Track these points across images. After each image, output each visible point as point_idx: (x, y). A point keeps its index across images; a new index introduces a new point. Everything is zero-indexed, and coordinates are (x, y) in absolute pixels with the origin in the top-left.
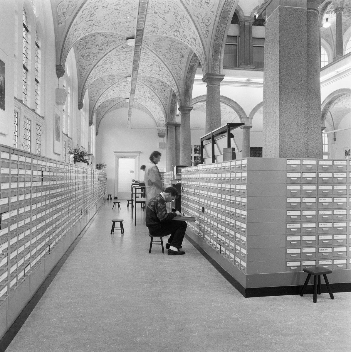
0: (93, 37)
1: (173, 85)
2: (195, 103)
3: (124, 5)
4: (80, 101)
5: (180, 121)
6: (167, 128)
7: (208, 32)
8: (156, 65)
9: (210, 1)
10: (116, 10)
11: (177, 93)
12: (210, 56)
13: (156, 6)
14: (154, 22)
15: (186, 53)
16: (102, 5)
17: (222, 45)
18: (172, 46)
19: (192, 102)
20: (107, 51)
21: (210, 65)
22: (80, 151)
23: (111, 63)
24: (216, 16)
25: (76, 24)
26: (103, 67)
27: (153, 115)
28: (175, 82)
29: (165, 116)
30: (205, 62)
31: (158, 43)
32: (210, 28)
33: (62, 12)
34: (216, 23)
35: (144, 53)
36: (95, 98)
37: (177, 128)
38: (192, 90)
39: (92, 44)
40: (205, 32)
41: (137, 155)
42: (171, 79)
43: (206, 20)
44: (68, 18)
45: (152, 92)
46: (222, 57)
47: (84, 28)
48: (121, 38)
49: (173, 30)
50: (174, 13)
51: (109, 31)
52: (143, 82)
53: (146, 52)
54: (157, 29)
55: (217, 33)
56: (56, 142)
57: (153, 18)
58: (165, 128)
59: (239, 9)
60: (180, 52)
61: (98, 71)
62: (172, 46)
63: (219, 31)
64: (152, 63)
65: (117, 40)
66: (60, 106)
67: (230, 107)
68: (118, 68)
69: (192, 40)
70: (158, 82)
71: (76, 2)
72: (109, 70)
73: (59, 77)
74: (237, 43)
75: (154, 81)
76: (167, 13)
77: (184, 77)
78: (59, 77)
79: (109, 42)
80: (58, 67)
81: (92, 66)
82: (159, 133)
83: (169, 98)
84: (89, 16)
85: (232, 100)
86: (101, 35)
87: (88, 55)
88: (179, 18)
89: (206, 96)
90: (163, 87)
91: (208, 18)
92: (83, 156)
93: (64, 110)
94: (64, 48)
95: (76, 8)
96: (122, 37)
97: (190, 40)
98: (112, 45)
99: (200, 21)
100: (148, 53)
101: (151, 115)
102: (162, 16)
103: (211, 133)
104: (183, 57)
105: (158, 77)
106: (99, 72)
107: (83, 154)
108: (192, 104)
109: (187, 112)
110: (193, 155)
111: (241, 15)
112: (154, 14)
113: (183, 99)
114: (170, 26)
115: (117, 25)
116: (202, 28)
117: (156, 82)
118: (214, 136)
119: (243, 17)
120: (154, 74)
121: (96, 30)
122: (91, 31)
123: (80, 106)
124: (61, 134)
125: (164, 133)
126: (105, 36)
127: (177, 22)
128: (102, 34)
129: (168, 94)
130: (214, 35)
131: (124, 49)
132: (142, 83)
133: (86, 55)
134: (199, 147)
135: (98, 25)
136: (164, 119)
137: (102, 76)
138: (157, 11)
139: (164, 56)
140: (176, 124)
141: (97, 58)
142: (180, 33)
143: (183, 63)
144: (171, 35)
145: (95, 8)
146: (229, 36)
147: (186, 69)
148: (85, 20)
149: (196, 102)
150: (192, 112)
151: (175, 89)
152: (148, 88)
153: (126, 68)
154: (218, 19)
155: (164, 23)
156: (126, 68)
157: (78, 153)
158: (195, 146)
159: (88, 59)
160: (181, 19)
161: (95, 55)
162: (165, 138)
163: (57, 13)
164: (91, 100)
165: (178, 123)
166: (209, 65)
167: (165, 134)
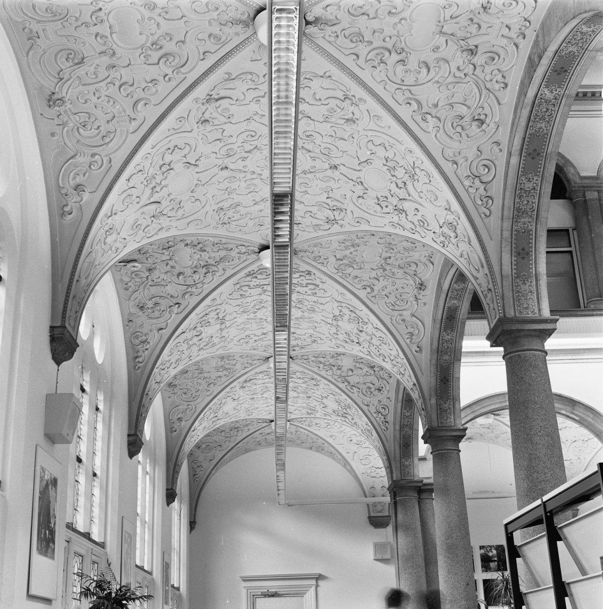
0: (166, 253)
1: (402, 370)
2: (471, 420)
3: (246, 155)
4: (133, 432)
5: (431, 474)
6: (395, 498)
7: (490, 201)
8: (346, 317)
9: (486, 115)
10: (222, 169)
11: (416, 392)
12: (504, 267)
13: (332, 147)
14: (331, 195)
15: (430, 275)
16: (185, 160)
17: (538, 233)
18: (390, 258)
19: (462, 416)
20: (207, 288)
21: (508, 294)
22: (115, 587)
23: (222, 321)
24: (510, 154)
25: (112, 214)
26: (198, 334)
27: (352, 463)
28: (405, 361)
29: (386, 463)
30: (491, 286)
31: (347, 252)
32: (497, 189)
33: (72, 183)
34: (509, 182)
35: (312, 287)
36: (183, 423)
37: (424, 496)
38: (459, 378)
39: (166, 273)
40: (480, 203)
41: (310, 586)
42: (394, 353)
43: (482, 168)
44: (89, 199)
45: (344, 396)
46: (542, 268)
47: (136, 226)
48: (243, 250)
49: (387, 210)
50: (385, 162)
51: (210, 231)
52: (316, 369)
53: (318, 282)
54: (343, 214)
55: (517, 200)
56: (38, 559)
57: (328, 184)
58: (388, 499)
59: (563, 162)
60: (412, 273)
61: (185, 346)
62: (390, 258)
63: (525, 195)
64: (337, 313)
65: (233, 254)
66: (59, 447)
67: (575, 425)
68: (243, 336)
69: (445, 230)
70: (358, 365)
71: (111, 154)
72: (216, 340)
73: (58, 362)
74: (570, 246)
75: (346, 363)
76: (364, 164)
77: (432, 344)
78: (58, 362)
79: (211, 262)
80: (55, 332)
81: (166, 333)
82: (372, 514)
83: (392, 411)
84: (148, 191)
85: (579, 403)
86: (187, 245)
87: (156, 304)
88: (400, 173)
89: (507, 397)
90: (375, 381)
91: (486, 162)
92: (124, 602)
93: (79, 460)
94: (76, 278)
95: (111, 169)
96: (246, 244)
97: (438, 230)
98: (221, 272)
99: (463, 171)
100: (321, 286)
101: (346, 464)
102: (354, 175)
103: (538, 502)
104: (422, 286)
105: (356, 350)
106: (189, 348)
107: (126, 594)
108: (463, 422)
109: (450, 445)
110: (480, 576)
111: (570, 176)
112: (329, 173)
113: (434, 406)
114: (379, 200)
115: (230, 213)
116: (471, 190)
117: (352, 368)
118: (551, 512)
119: (578, 180)
120: (344, 344)
121: (173, 229)
122: (156, 234)
123: (134, 445)
124: (61, 534)
125: (387, 514)
126: (198, 245)
127: (397, 186)
128: (189, 242)
129: (389, 398)
130: (510, 208)
131: (254, 280)
132: (313, 372)
133: (150, 304)
134: (495, 552)
135: (175, 215)
136: (383, 472)
137: (198, 358)
138: (337, 162)
139: (369, 290)
140: (420, 484)
141: (179, 310)
142: (406, 215)
143: (425, 304)
144: (382, 223)
145: (164, 169)
146: (551, 232)
147: (434, 320)
148: (138, 203)
149: (472, 416)
150: (462, 445)
151: (408, 381)
152: (332, 386)
153: (264, 334)
154: (514, 160)
155: (361, 194)
156: (264, 334)
157: (110, 593)
158: (482, 547)
159: (157, 314)
160: (407, 175)
161: (175, 301)
162: (390, 529)
163: (59, 188)
164: (170, 429)
165: (425, 481)
166: (503, 294)
167: (389, 516)
